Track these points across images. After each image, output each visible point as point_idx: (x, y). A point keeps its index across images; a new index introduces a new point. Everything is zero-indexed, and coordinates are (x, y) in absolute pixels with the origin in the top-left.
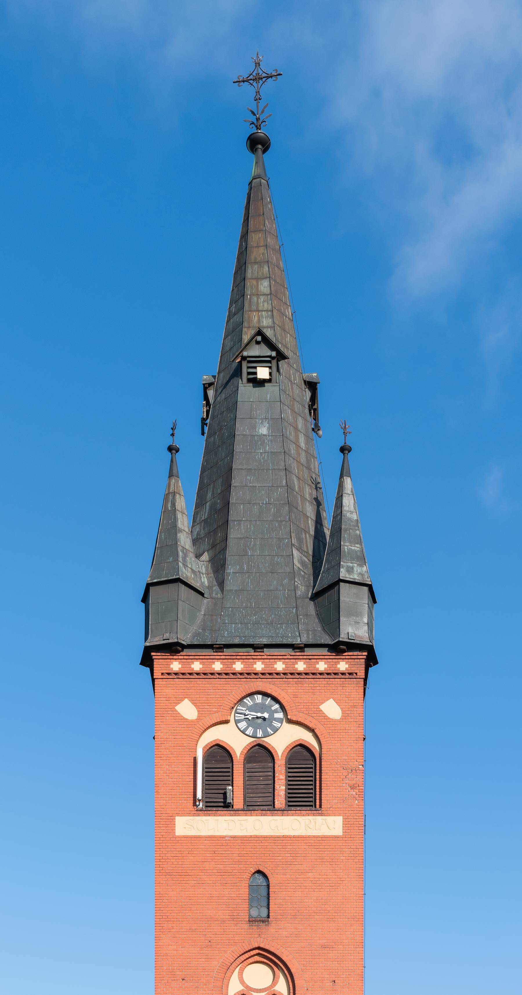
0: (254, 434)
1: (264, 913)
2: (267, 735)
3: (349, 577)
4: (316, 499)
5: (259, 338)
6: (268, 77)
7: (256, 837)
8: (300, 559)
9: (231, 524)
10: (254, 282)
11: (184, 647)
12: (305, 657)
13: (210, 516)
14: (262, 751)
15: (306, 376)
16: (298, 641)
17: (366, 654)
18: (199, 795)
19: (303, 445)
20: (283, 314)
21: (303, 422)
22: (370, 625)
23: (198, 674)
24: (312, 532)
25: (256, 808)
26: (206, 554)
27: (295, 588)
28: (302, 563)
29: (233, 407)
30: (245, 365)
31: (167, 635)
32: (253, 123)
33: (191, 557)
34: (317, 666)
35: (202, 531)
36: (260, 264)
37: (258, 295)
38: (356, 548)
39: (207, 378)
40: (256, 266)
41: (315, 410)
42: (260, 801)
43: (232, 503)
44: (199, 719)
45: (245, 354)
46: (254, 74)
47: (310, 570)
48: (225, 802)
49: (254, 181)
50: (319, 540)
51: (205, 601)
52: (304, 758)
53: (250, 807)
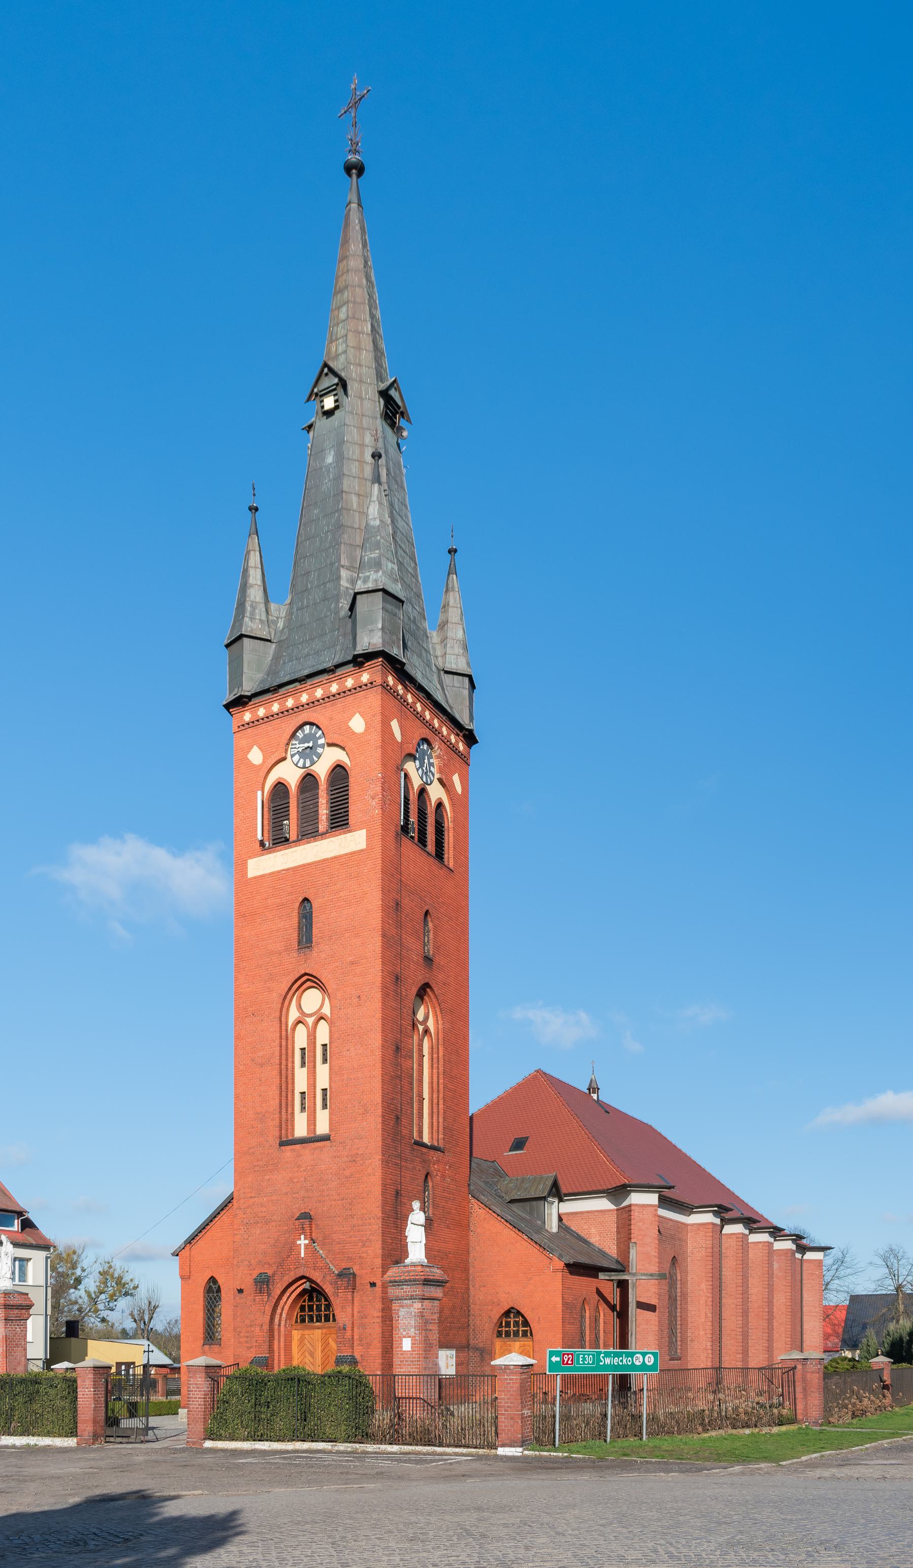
44: (264, 762)
51: (274, 646)
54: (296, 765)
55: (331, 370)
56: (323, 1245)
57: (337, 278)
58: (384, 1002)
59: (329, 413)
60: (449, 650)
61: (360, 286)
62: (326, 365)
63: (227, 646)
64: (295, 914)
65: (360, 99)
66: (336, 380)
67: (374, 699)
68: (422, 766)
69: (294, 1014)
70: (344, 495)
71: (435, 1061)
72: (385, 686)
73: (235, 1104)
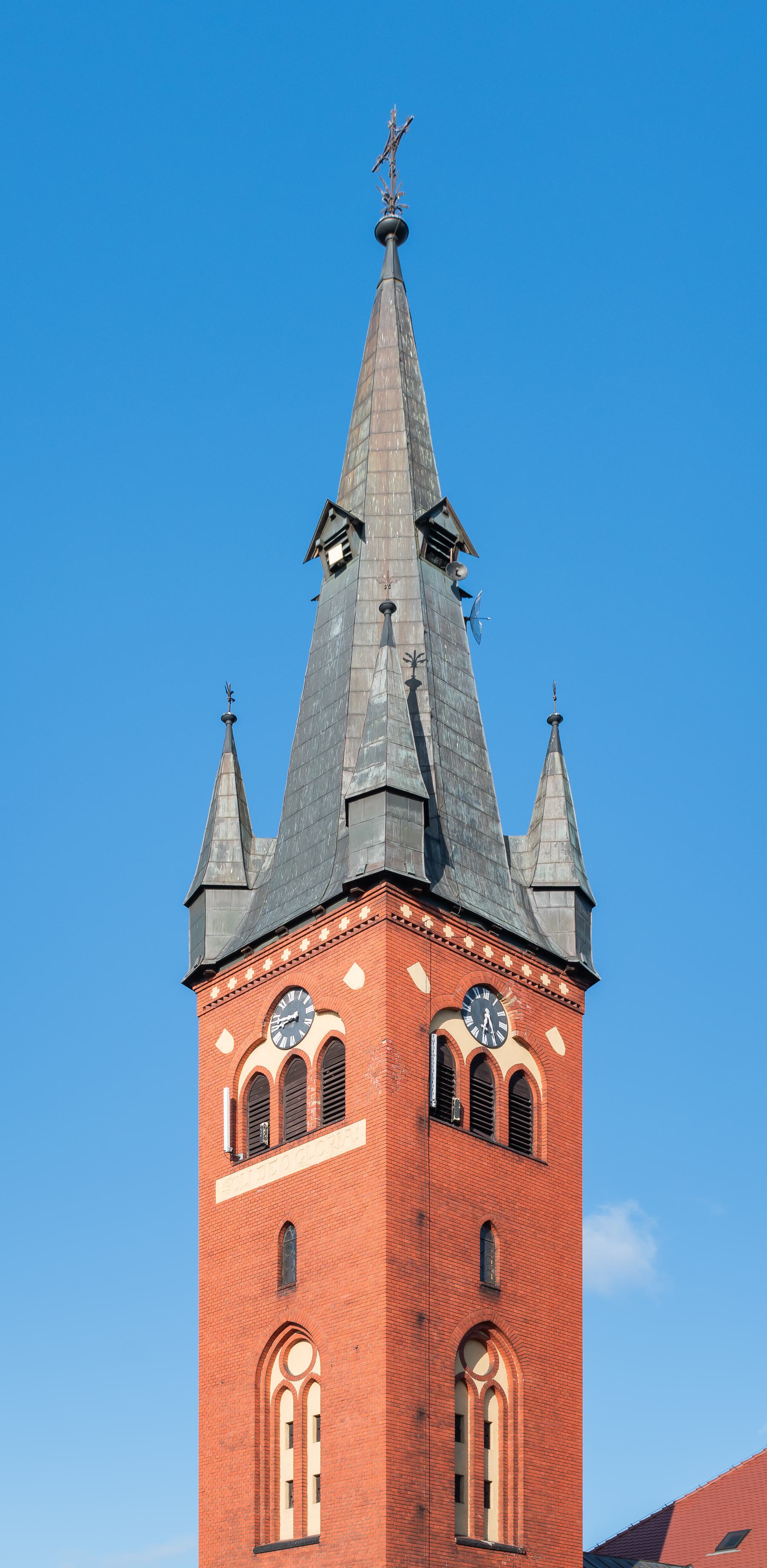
2: (299, 1040)
12: (327, 921)
44: (236, 1048)
54: (278, 1046)
55: (338, 510)
57: (360, 386)
58: (391, 1351)
59: (337, 569)
60: (541, 859)
61: (392, 387)
62: (331, 505)
63: (189, 904)
64: (275, 1245)
65: (399, 138)
66: (345, 521)
67: (377, 941)
68: (478, 1022)
69: (277, 1378)
70: (353, 673)
71: (510, 1429)
72: (395, 920)
73: (201, 1501)
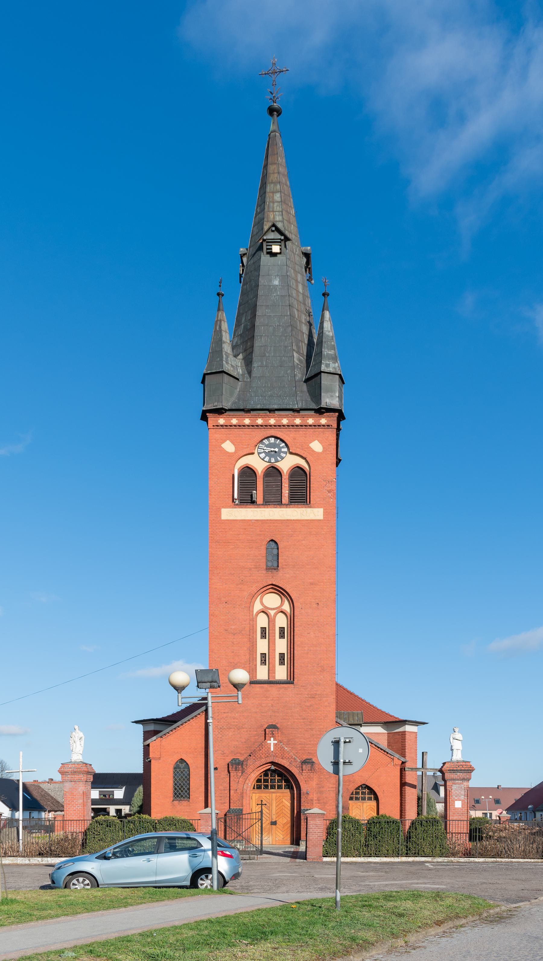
0: (270, 284)
1: (276, 565)
2: (277, 461)
3: (327, 370)
4: (309, 322)
5: (273, 229)
6: (280, 72)
7: (271, 520)
8: (298, 358)
9: (256, 338)
10: (271, 195)
11: (226, 410)
13: (243, 332)
14: (275, 470)
15: (303, 249)
16: (296, 407)
17: (337, 414)
18: (236, 496)
19: (301, 290)
20: (289, 213)
21: (301, 277)
22: (340, 398)
23: (235, 426)
24: (306, 342)
25: (270, 503)
26: (241, 354)
27: (295, 376)
28: (300, 360)
29: (257, 268)
30: (265, 244)
31: (216, 404)
32: (271, 99)
33: (231, 358)
34: (308, 421)
35: (239, 341)
36: (275, 183)
37: (273, 202)
38: (332, 352)
39: (242, 250)
40: (272, 185)
41: (309, 268)
42: (273, 500)
43: (258, 316)
44: (235, 452)
45: (265, 238)
46: (272, 70)
47: (304, 364)
48: (252, 500)
49: (272, 134)
50: (311, 346)
51: (240, 383)
52: (299, 475)
53: (267, 503)
56: (288, 744)
